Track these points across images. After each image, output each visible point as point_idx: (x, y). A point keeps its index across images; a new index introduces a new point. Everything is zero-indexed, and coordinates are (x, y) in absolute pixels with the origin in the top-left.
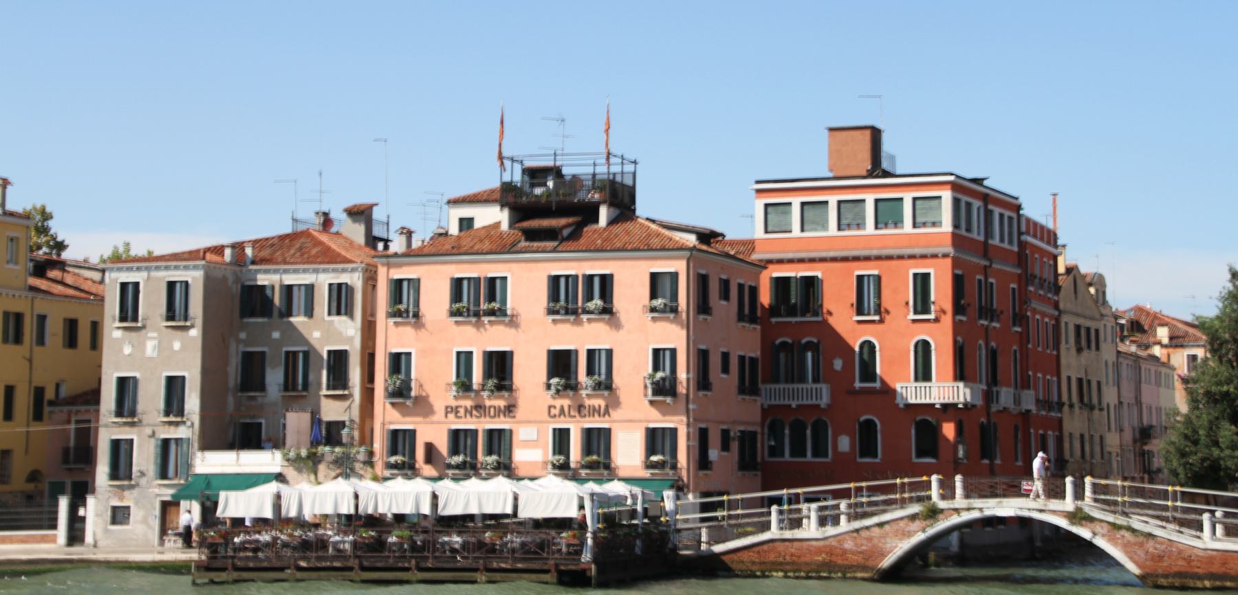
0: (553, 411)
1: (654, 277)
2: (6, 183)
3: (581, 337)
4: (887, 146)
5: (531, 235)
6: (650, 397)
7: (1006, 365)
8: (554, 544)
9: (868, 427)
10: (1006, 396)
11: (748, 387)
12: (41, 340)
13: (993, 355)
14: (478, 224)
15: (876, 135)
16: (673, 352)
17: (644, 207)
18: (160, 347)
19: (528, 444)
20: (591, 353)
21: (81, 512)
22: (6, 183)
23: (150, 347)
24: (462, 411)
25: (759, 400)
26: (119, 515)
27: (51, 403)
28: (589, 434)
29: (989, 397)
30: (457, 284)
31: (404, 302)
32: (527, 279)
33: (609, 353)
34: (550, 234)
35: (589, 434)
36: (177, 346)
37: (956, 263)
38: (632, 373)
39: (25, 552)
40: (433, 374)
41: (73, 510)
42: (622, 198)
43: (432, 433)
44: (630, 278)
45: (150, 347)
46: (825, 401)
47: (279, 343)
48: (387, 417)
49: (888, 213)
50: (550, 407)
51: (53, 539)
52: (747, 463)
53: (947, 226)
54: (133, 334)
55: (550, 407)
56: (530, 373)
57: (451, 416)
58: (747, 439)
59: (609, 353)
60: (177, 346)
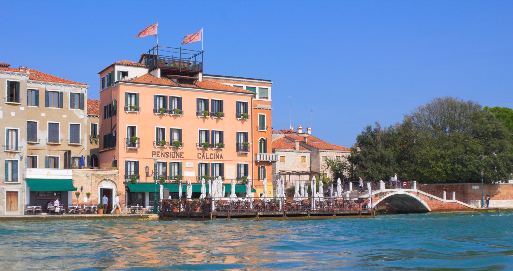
0: (200, 156)
20: (213, 132)
38: (230, 141)
50: (198, 154)
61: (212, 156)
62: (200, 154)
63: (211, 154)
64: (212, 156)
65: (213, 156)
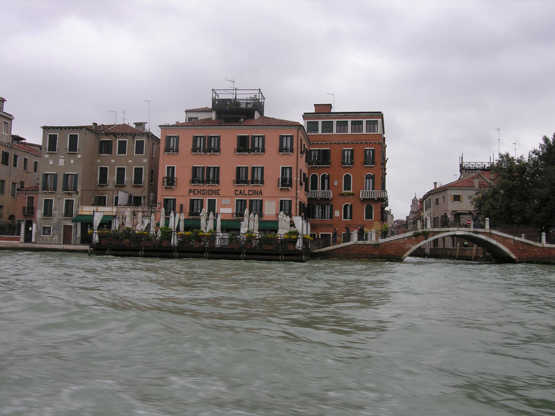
0: (237, 192)
2: (3, 100)
3: (249, 161)
6: (280, 187)
12: (15, 165)
16: (291, 168)
19: (225, 206)
20: (253, 168)
21: (30, 229)
22: (3, 100)
23: (61, 162)
24: (196, 192)
27: (18, 190)
28: (324, 189)
30: (195, 138)
32: (229, 137)
33: (262, 168)
35: (324, 189)
36: (72, 161)
39: (11, 159)
40: (183, 176)
45: (61, 162)
47: (114, 165)
48: (162, 194)
50: (236, 190)
51: (18, 239)
54: (54, 155)
55: (236, 190)
56: (227, 176)
57: (191, 194)
59: (262, 168)
60: (72, 161)
61: (250, 193)
62: (238, 191)
63: (249, 191)
64: (250, 193)
65: (252, 193)
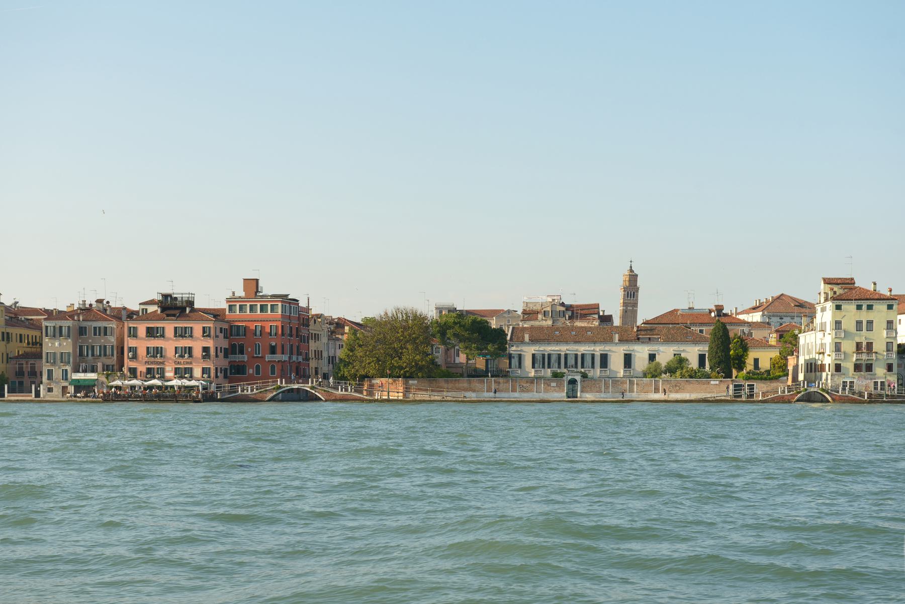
1: (204, 328)
4: (260, 284)
5: (168, 315)
7: (295, 349)
8: (407, 321)
9: (258, 367)
10: (294, 358)
11: (226, 356)
13: (291, 346)
14: (149, 312)
15: (257, 280)
17: (196, 306)
18: (60, 345)
19: (169, 372)
25: (229, 360)
26: (50, 390)
29: (290, 358)
31: (133, 333)
32: (169, 327)
34: (174, 315)
37: (282, 322)
38: (198, 352)
41: (36, 389)
42: (191, 303)
43: (142, 368)
44: (198, 328)
46: (246, 359)
49: (263, 309)
52: (225, 377)
53: (280, 312)
58: (226, 370)
